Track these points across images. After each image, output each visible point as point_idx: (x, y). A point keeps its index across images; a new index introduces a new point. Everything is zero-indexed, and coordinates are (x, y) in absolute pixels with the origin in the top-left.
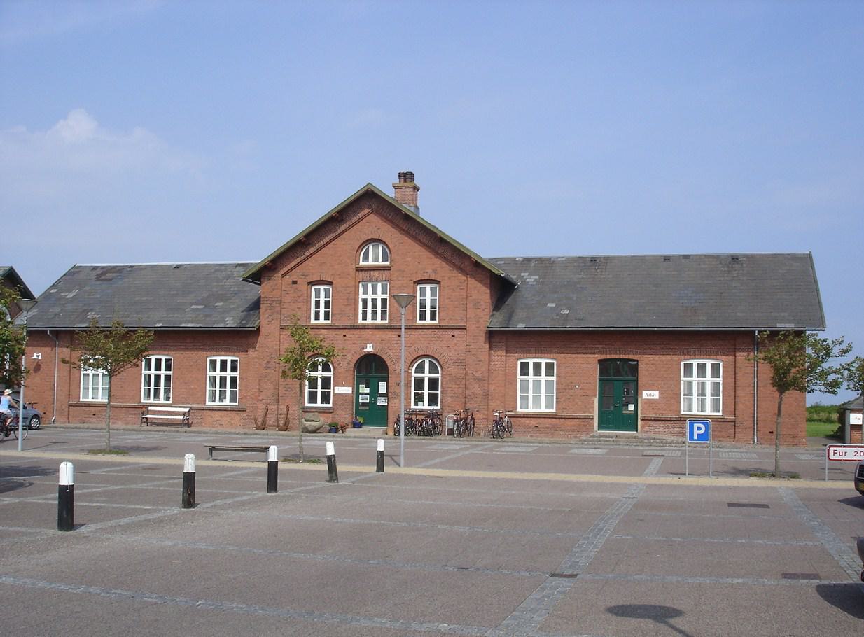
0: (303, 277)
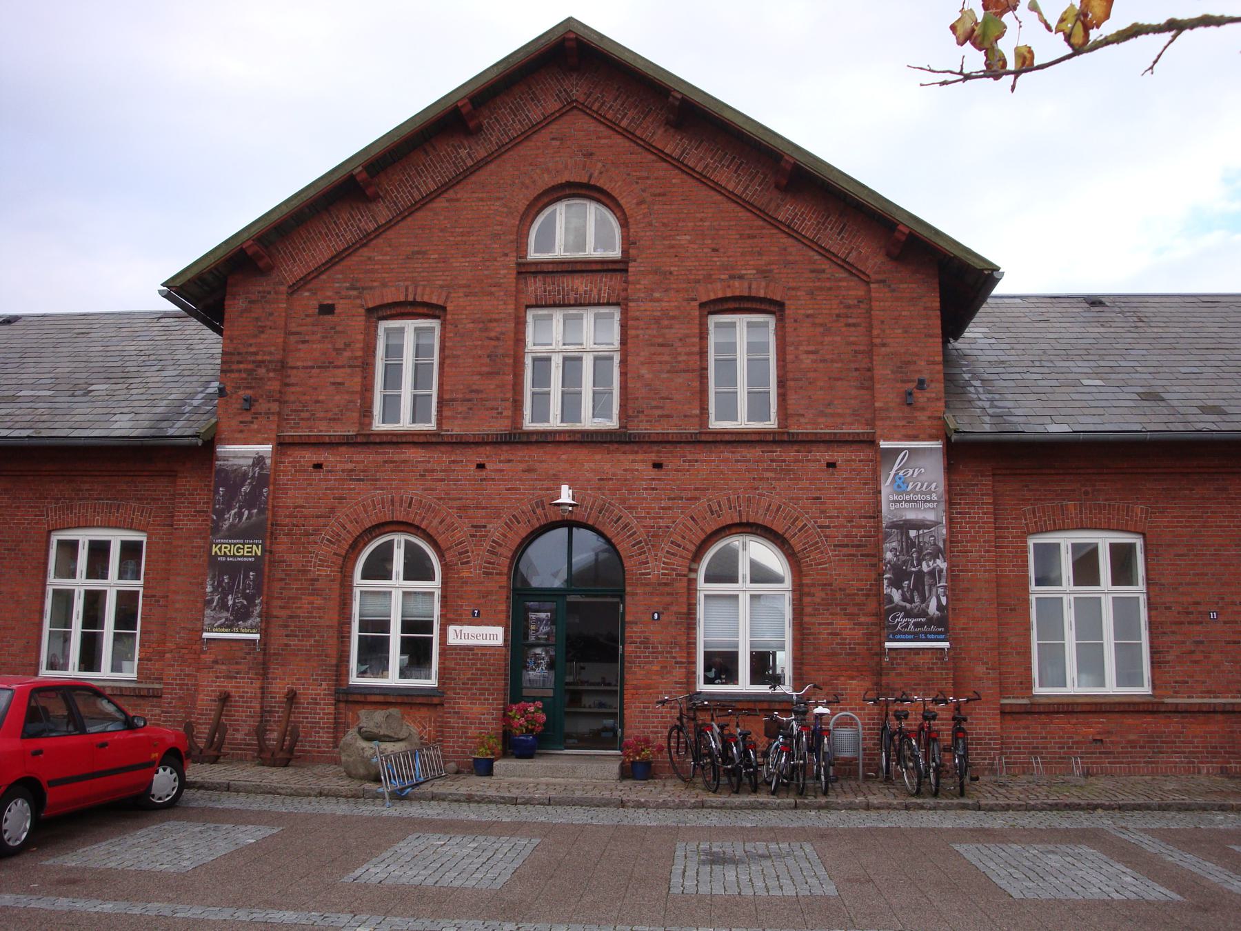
0: (355, 293)
